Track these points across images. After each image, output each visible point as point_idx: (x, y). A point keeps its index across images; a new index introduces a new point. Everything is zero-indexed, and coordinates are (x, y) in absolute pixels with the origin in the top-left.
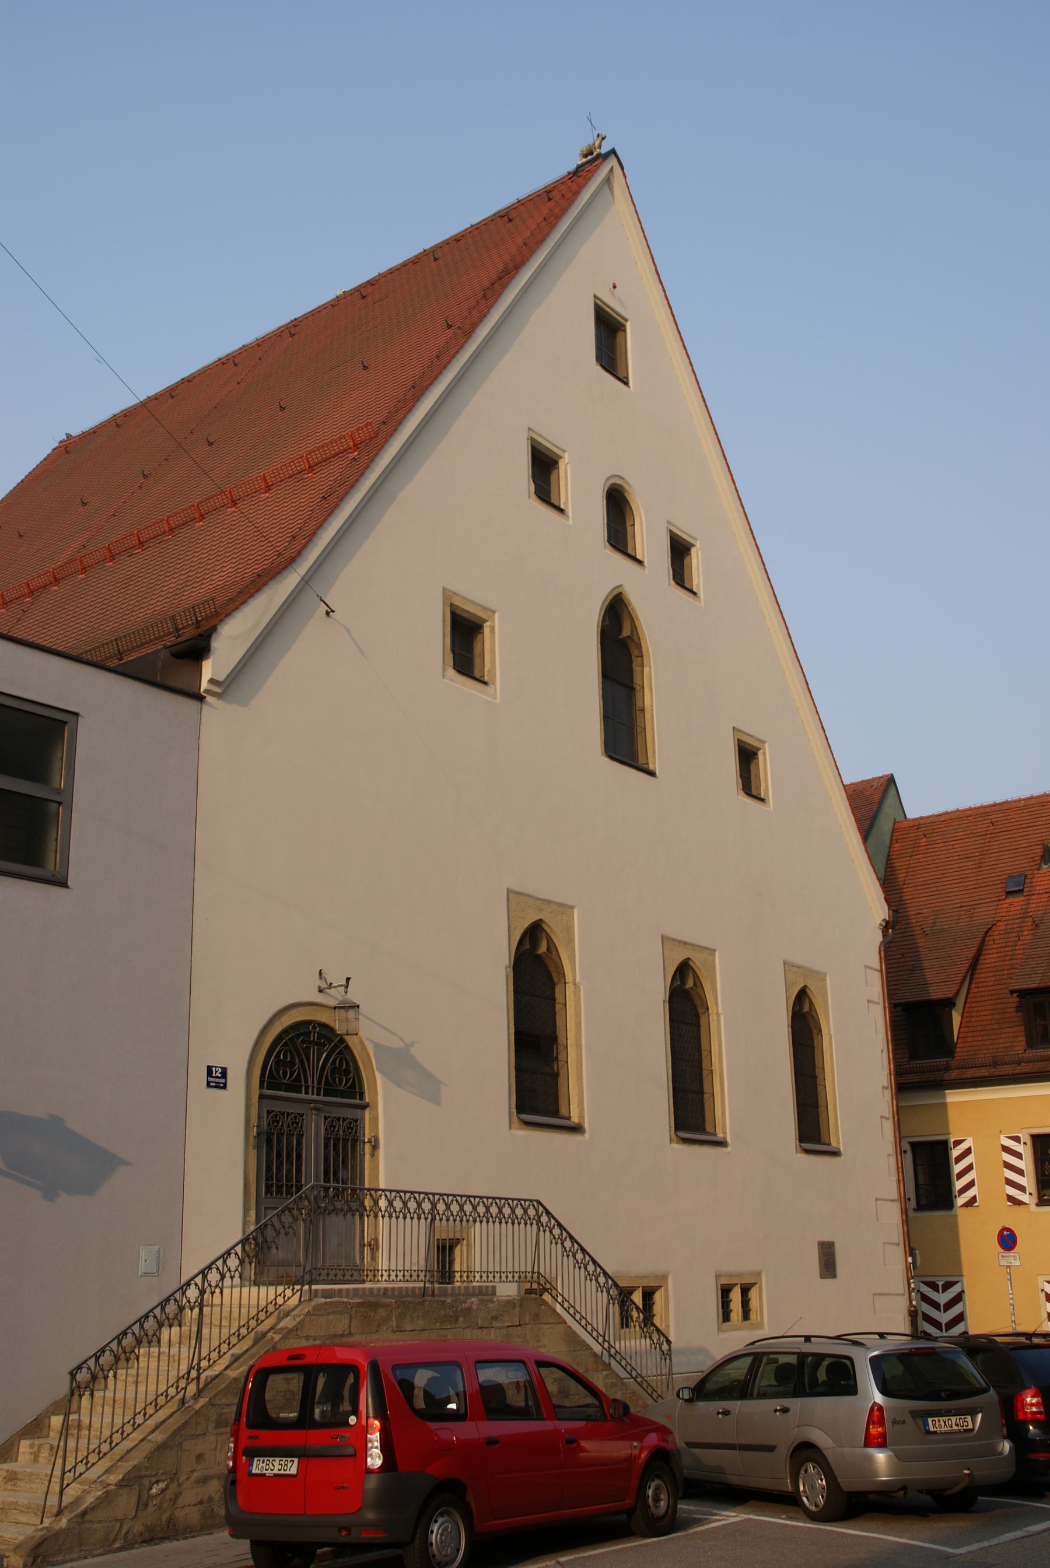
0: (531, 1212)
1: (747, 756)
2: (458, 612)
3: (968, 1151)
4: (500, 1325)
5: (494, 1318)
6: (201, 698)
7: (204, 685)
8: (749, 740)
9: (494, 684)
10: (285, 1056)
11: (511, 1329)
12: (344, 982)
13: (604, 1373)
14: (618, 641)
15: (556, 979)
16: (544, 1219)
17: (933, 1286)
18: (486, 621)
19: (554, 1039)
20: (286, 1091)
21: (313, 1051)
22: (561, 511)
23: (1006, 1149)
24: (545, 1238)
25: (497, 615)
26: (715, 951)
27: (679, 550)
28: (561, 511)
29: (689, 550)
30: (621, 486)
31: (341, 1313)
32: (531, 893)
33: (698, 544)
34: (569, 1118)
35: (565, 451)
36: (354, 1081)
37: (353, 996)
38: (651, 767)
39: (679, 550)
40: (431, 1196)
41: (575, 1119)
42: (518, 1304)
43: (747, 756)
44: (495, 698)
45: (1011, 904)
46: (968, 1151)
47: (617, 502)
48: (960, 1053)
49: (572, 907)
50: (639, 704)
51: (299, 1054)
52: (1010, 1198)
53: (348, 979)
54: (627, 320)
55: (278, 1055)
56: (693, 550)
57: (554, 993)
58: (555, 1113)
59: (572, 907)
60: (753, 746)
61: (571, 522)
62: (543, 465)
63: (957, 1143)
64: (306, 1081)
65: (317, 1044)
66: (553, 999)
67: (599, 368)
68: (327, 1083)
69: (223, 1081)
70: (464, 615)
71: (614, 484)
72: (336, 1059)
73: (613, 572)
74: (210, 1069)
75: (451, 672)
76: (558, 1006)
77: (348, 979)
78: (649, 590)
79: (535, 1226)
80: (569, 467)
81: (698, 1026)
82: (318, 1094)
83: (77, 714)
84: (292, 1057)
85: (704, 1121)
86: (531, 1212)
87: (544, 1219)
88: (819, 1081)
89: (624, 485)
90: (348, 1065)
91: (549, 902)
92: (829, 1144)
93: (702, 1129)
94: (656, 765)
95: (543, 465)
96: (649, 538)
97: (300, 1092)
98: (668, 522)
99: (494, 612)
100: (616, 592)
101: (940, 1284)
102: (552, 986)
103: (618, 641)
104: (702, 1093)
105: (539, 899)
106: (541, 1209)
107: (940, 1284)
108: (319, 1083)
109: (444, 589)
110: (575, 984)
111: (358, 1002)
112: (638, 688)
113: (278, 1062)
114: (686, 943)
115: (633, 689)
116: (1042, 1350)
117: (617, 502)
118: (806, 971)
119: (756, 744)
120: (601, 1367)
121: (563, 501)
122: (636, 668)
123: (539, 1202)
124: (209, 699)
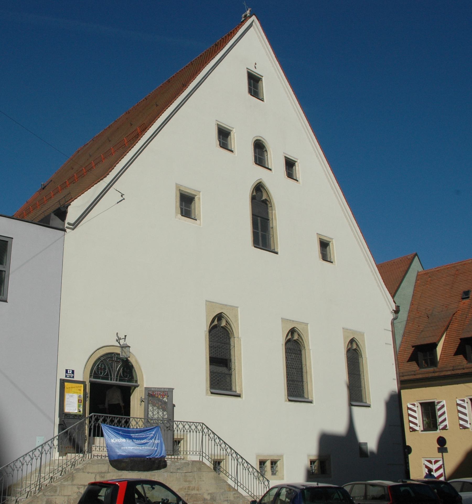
0: (199, 427)
1: (324, 245)
2: (183, 193)
3: (443, 406)
4: (181, 472)
5: (178, 469)
6: (65, 231)
7: (66, 225)
8: (325, 238)
9: (200, 220)
10: (101, 366)
11: (187, 474)
12: (124, 337)
13: (234, 492)
14: (260, 202)
15: (231, 336)
16: (206, 430)
17: (430, 462)
18: (196, 195)
19: (230, 360)
20: (102, 379)
21: (115, 364)
22: (232, 151)
23: (458, 405)
24: (206, 438)
25: (201, 193)
26: (308, 324)
27: (290, 164)
28: (232, 151)
29: (295, 164)
30: (260, 140)
31: (104, 464)
32: (217, 302)
33: (298, 161)
34: (236, 392)
35: (233, 128)
36: (108, 373)
37: (128, 342)
38: (276, 250)
39: (290, 164)
40: (201, 424)
41: (238, 392)
42: (191, 464)
43: (324, 245)
44: (200, 225)
45: (464, 303)
46: (443, 406)
47: (259, 147)
48: (439, 365)
49: (237, 307)
50: (271, 226)
51: (108, 365)
52: (461, 425)
53: (125, 336)
54: (262, 77)
55: (98, 365)
56: (296, 163)
57: (230, 342)
58: (231, 389)
59: (237, 307)
60: (327, 241)
61: (236, 155)
62: (224, 135)
63: (439, 403)
64: (111, 376)
65: (116, 361)
66: (229, 344)
67: (250, 95)
68: (120, 377)
69: (72, 375)
70: (186, 194)
71: (257, 140)
72: (99, 365)
73: (259, 174)
74: (67, 371)
75: (180, 216)
76: (231, 347)
77: (125, 336)
78: (275, 180)
79: (201, 433)
80: (235, 134)
81: (301, 354)
82: (116, 381)
83: (12, 238)
84: (105, 366)
85: (303, 393)
86: (199, 427)
87: (206, 430)
88: (362, 377)
89: (263, 140)
90: (105, 366)
91: (226, 305)
92: (366, 403)
93: (361, 401)
94: (279, 250)
95: (224, 135)
96: (275, 159)
97: (108, 380)
98: (284, 153)
99: (200, 192)
100: (258, 182)
101: (433, 461)
102: (229, 339)
103: (260, 202)
104: (302, 381)
105: (221, 304)
106: (204, 426)
107: (433, 461)
108: (117, 376)
109: (176, 184)
110: (238, 338)
111: (129, 345)
112: (270, 219)
113: (98, 368)
114: (293, 321)
115: (269, 220)
116: (42, 464)
117: (259, 147)
118: (354, 332)
119: (328, 240)
120: (232, 490)
121: (233, 147)
122: (270, 212)
123: (203, 424)
124: (68, 230)
